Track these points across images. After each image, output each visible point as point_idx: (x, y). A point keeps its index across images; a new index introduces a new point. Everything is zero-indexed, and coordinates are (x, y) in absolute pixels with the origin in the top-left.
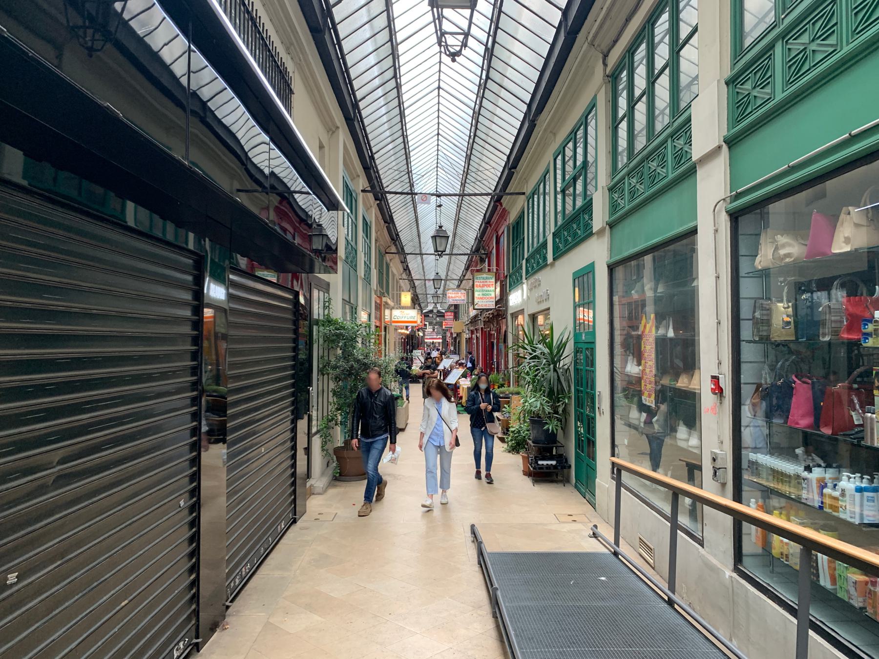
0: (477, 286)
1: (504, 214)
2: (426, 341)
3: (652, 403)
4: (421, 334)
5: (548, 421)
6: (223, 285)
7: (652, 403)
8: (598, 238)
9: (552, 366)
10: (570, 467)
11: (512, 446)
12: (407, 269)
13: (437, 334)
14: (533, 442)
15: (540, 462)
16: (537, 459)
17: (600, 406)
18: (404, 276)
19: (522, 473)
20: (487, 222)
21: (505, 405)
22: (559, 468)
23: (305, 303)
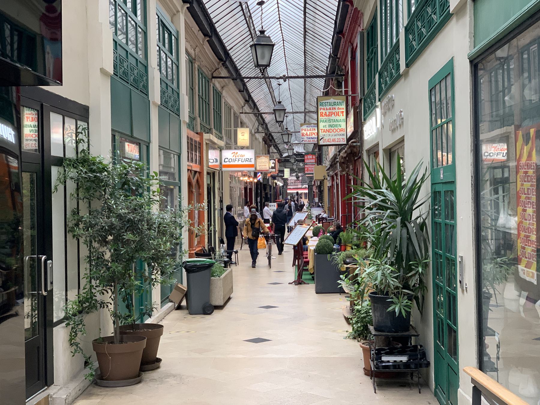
0: (322, 115)
1: (357, 15)
2: (288, 191)
3: (533, 277)
4: (280, 184)
5: (395, 300)
6: (10, 122)
7: (533, 277)
8: (457, 20)
9: (399, 219)
10: (428, 364)
11: (357, 330)
12: (249, 100)
13: (303, 182)
14: (376, 329)
15: (384, 358)
16: (379, 353)
17: (463, 278)
18: (247, 109)
19: (362, 372)
20: (339, 32)
21: (341, 276)
22: (413, 366)
23: (124, 147)
